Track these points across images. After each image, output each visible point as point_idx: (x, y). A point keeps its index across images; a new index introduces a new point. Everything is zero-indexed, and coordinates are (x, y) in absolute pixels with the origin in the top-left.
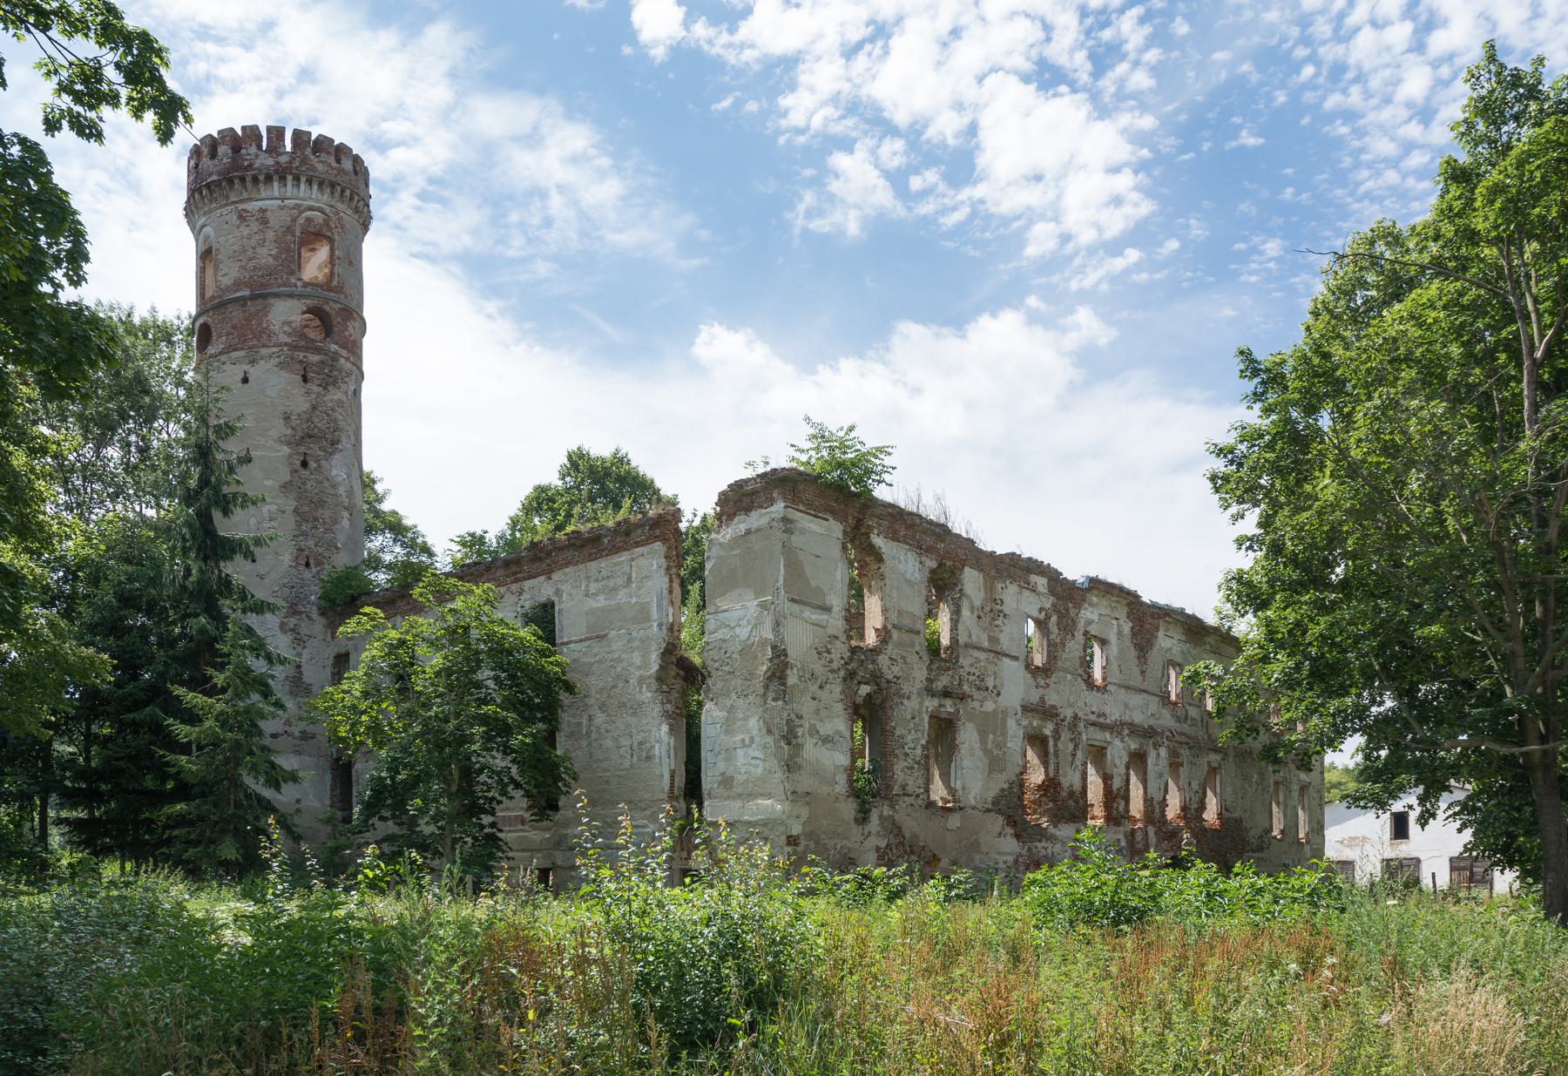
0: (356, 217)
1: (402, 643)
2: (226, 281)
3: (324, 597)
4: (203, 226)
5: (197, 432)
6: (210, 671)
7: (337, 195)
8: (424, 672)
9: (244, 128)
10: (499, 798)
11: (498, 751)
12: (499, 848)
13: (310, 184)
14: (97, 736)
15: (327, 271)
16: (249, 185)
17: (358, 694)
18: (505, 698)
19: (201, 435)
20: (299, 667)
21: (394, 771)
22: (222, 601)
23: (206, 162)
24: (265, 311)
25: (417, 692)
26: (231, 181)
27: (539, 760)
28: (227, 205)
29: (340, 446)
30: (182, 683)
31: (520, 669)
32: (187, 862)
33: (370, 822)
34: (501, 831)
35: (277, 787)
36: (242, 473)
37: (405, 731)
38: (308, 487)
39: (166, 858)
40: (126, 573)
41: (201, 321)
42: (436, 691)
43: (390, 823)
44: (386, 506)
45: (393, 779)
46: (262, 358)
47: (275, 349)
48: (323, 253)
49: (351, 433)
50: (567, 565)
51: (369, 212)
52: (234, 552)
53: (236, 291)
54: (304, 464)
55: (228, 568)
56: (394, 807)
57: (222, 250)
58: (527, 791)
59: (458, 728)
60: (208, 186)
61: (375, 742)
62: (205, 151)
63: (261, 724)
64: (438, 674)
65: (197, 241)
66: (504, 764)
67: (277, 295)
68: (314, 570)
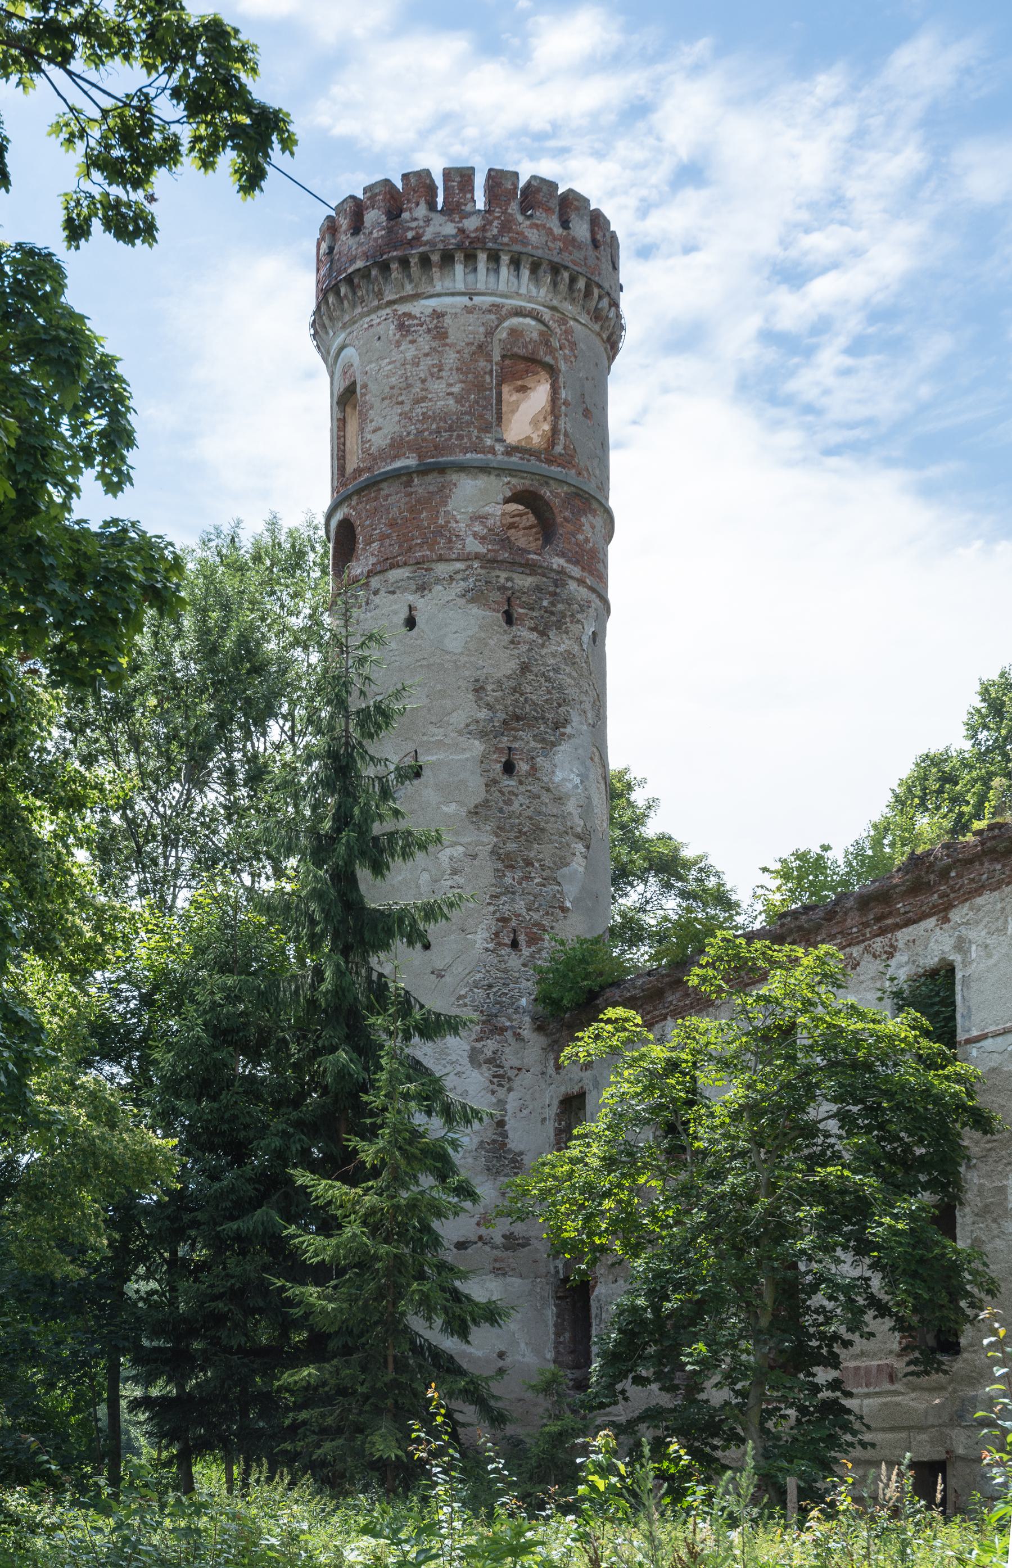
0: (597, 327)
1: (673, 1066)
2: (379, 441)
3: (544, 999)
4: (342, 348)
5: (331, 728)
6: (354, 1142)
7: (563, 287)
8: (712, 1115)
9: (405, 177)
10: (847, 1336)
11: (845, 1248)
12: (846, 1427)
13: (517, 268)
14: (185, 1262)
15: (547, 427)
16: (415, 270)
17: (596, 1163)
18: (860, 1152)
19: (337, 733)
20: (501, 1124)
21: (657, 1296)
22: (372, 1020)
23: (346, 241)
24: (443, 493)
25: (697, 1151)
26: (385, 267)
27: (922, 1261)
28: (378, 308)
29: (568, 730)
30: (314, 1167)
31: (889, 1095)
32: (323, 1464)
33: (619, 1387)
34: (849, 1395)
35: (463, 1333)
36: (405, 796)
37: (678, 1223)
38: (516, 806)
39: (290, 1459)
40: (223, 988)
41: (339, 516)
42: (733, 1147)
43: (655, 1387)
44: (651, 830)
45: (657, 1309)
46: (438, 581)
47: (459, 565)
48: (539, 395)
49: (587, 706)
50: (978, 891)
51: (619, 316)
52: (390, 933)
53: (396, 457)
54: (509, 768)
55: (381, 963)
56: (659, 1359)
57: (372, 386)
58: (900, 1320)
59: (770, 1212)
60: (349, 280)
61: (625, 1245)
62: (344, 223)
63: (436, 1224)
64: (736, 1116)
65: (332, 375)
66: (856, 1273)
67: (462, 468)
68: (526, 952)
